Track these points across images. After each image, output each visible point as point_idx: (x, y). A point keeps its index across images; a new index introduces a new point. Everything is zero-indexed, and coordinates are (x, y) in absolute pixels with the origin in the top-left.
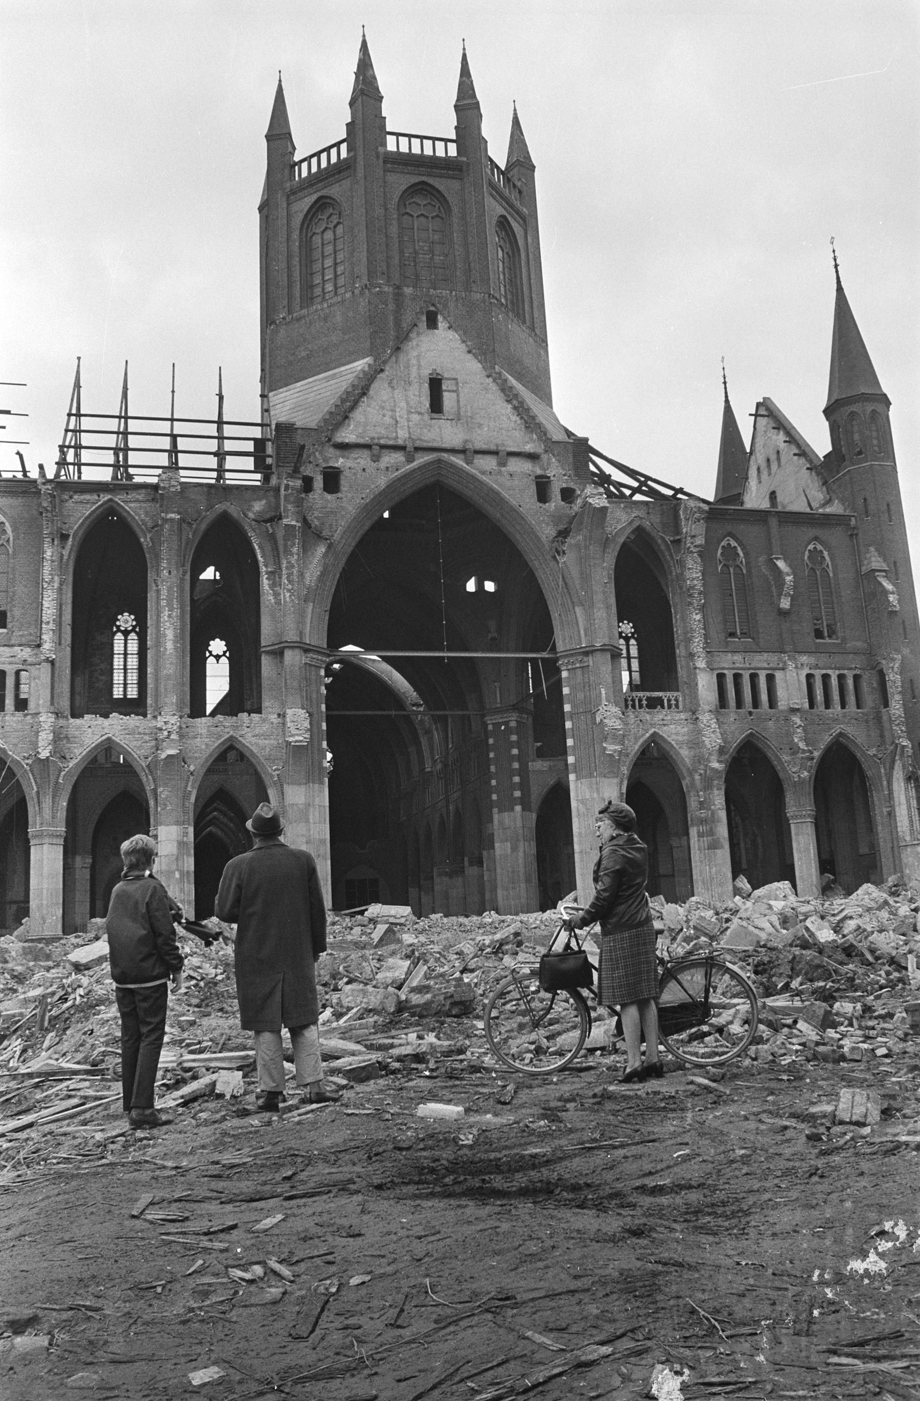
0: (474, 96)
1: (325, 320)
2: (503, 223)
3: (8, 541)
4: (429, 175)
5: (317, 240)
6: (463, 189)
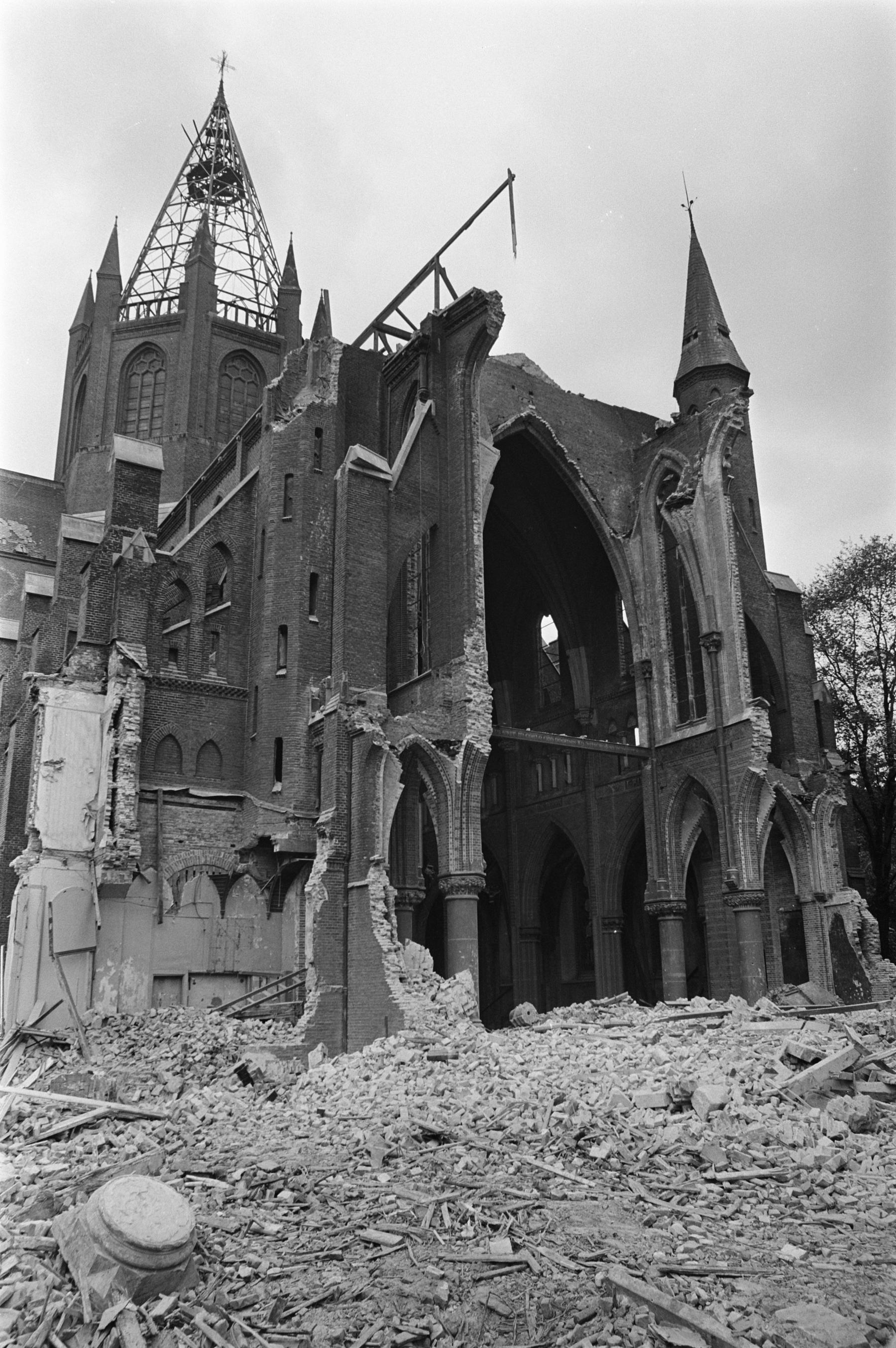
4: (249, 345)
5: (136, 380)
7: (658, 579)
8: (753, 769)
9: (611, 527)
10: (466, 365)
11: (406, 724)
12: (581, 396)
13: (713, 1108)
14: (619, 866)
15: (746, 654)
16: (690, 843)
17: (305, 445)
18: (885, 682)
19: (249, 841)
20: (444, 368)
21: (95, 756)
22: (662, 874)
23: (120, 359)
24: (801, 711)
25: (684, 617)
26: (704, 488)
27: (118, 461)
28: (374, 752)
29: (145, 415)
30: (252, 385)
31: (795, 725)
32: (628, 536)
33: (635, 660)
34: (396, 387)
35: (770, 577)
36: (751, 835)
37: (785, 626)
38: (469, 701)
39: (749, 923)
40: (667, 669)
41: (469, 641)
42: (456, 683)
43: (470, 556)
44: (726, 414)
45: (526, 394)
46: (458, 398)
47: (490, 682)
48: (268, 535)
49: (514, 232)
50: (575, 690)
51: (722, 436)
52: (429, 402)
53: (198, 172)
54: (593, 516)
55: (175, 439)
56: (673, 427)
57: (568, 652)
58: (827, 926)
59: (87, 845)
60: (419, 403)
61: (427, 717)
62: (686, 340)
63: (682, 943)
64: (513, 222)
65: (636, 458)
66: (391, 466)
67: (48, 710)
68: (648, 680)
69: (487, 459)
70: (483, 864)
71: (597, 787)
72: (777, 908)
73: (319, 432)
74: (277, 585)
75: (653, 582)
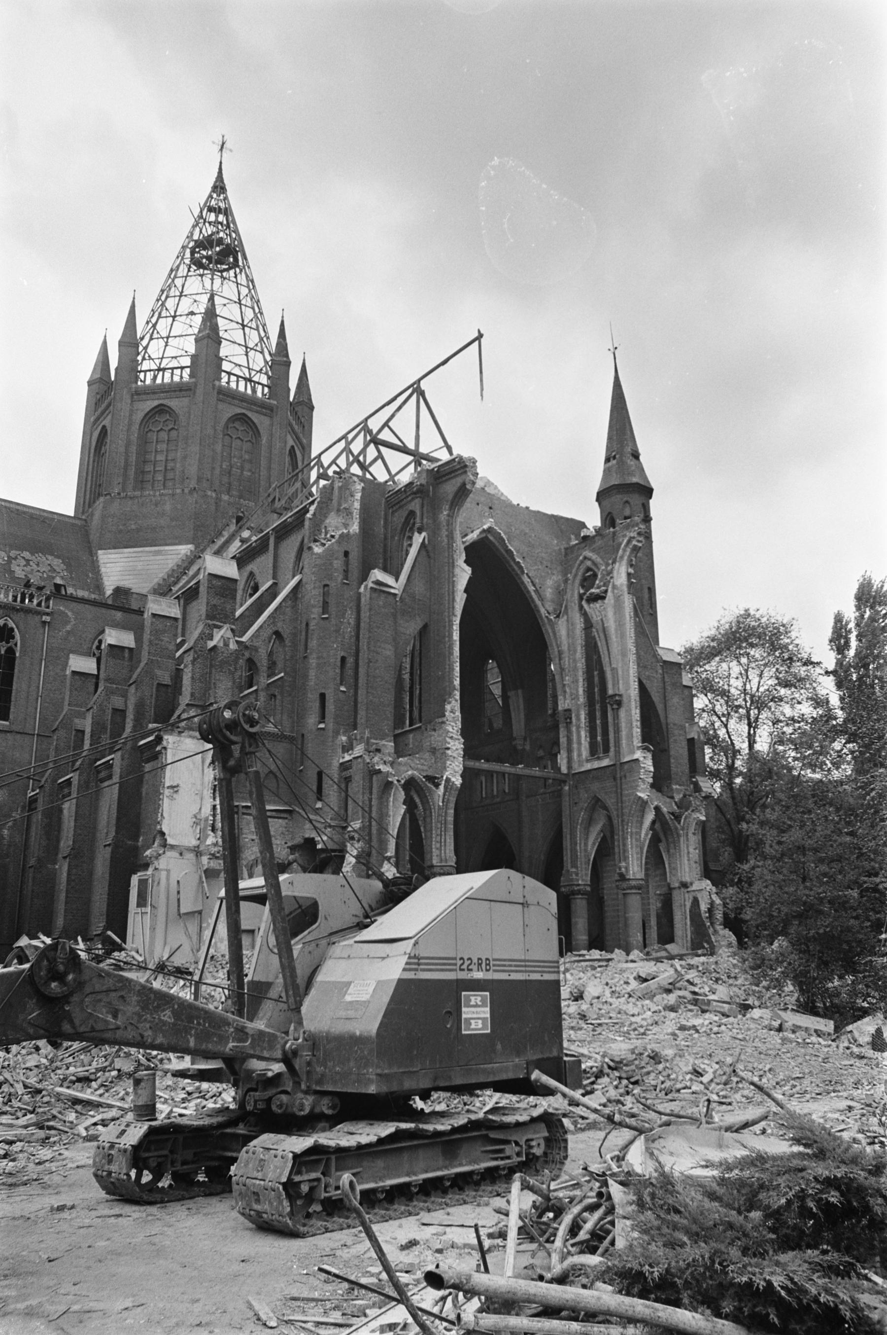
0: (287, 356)
1: (156, 505)
2: (292, 450)
3: (16, 645)
6: (272, 425)
7: (579, 648)
8: (639, 794)
9: (544, 609)
10: (450, 509)
11: (405, 764)
12: (527, 508)
13: (594, 998)
14: (542, 857)
15: (638, 711)
16: (594, 844)
17: (338, 564)
18: (749, 719)
19: (298, 840)
20: (434, 506)
21: (199, 782)
22: (574, 865)
23: (140, 416)
24: (678, 751)
25: (596, 679)
26: (614, 587)
27: (210, 574)
28: (388, 785)
29: (160, 468)
30: (249, 444)
31: (672, 761)
32: (558, 616)
33: (560, 708)
34: (396, 511)
35: (660, 652)
36: (637, 840)
37: (669, 688)
38: (448, 749)
39: (634, 901)
40: (583, 716)
41: (448, 707)
42: (439, 736)
43: (451, 647)
44: (632, 535)
45: (487, 509)
46: (444, 533)
47: (462, 735)
48: (311, 628)
49: (481, 380)
50: (514, 722)
51: (629, 550)
52: (424, 534)
53: (202, 244)
54: (533, 601)
55: (186, 491)
56: (594, 537)
57: (509, 694)
58: (688, 904)
59: (194, 843)
60: (416, 534)
61: (420, 759)
62: (607, 460)
63: (586, 916)
64: (481, 372)
65: (566, 554)
66: (397, 580)
67: (169, 751)
68: (569, 724)
69: (463, 574)
70: (454, 859)
71: (528, 797)
72: (655, 892)
73: (346, 554)
74: (318, 664)
75: (575, 651)
